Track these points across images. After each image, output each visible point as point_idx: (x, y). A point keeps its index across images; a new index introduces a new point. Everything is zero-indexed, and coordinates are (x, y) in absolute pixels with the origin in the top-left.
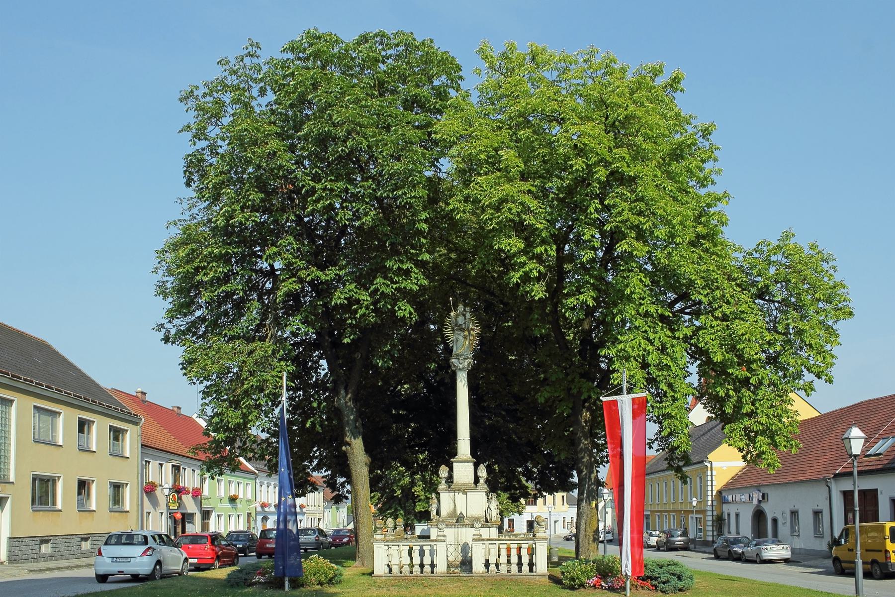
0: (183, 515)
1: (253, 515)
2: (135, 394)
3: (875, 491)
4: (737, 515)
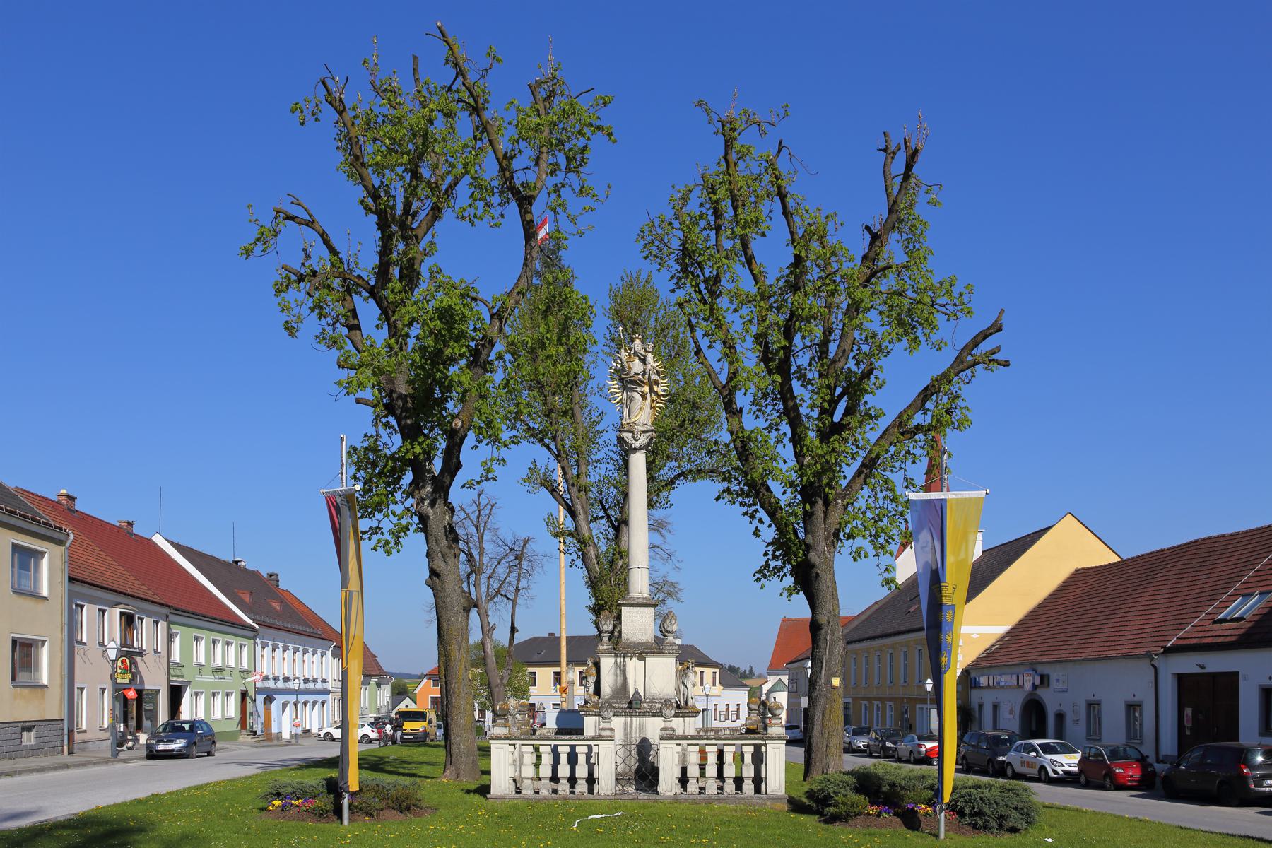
0: (140, 692)
1: (251, 693)
2: (56, 499)
3: (1235, 675)
4: (996, 707)
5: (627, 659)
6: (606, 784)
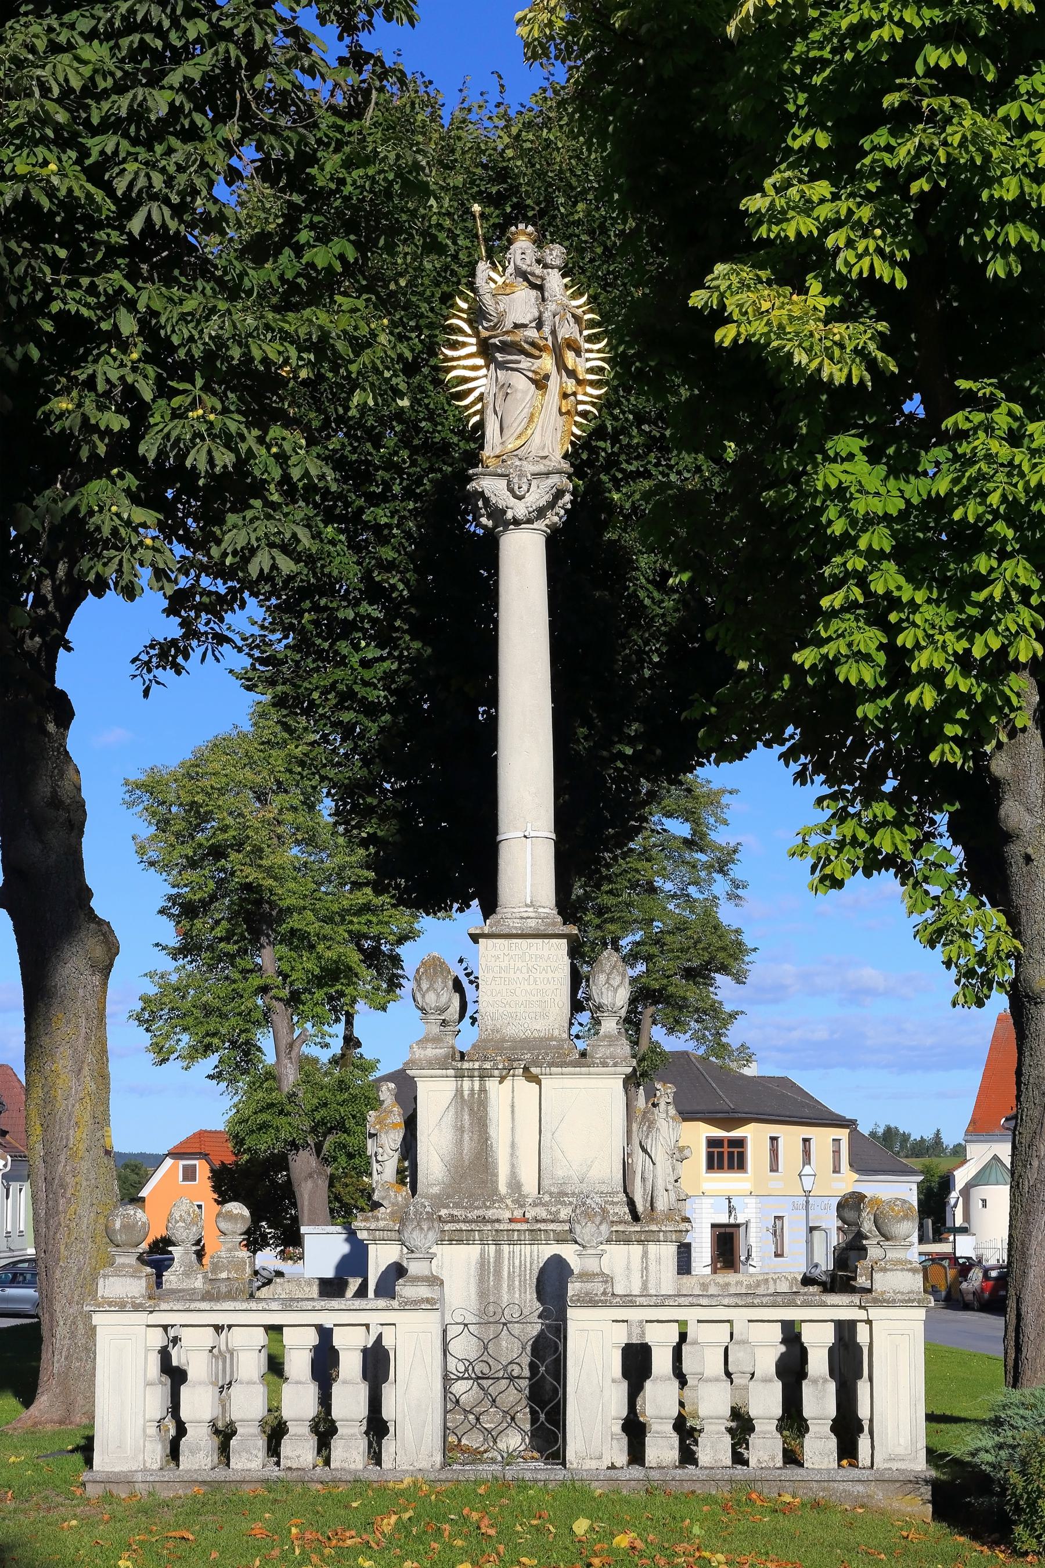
5: (492, 1084)
6: (416, 1442)
